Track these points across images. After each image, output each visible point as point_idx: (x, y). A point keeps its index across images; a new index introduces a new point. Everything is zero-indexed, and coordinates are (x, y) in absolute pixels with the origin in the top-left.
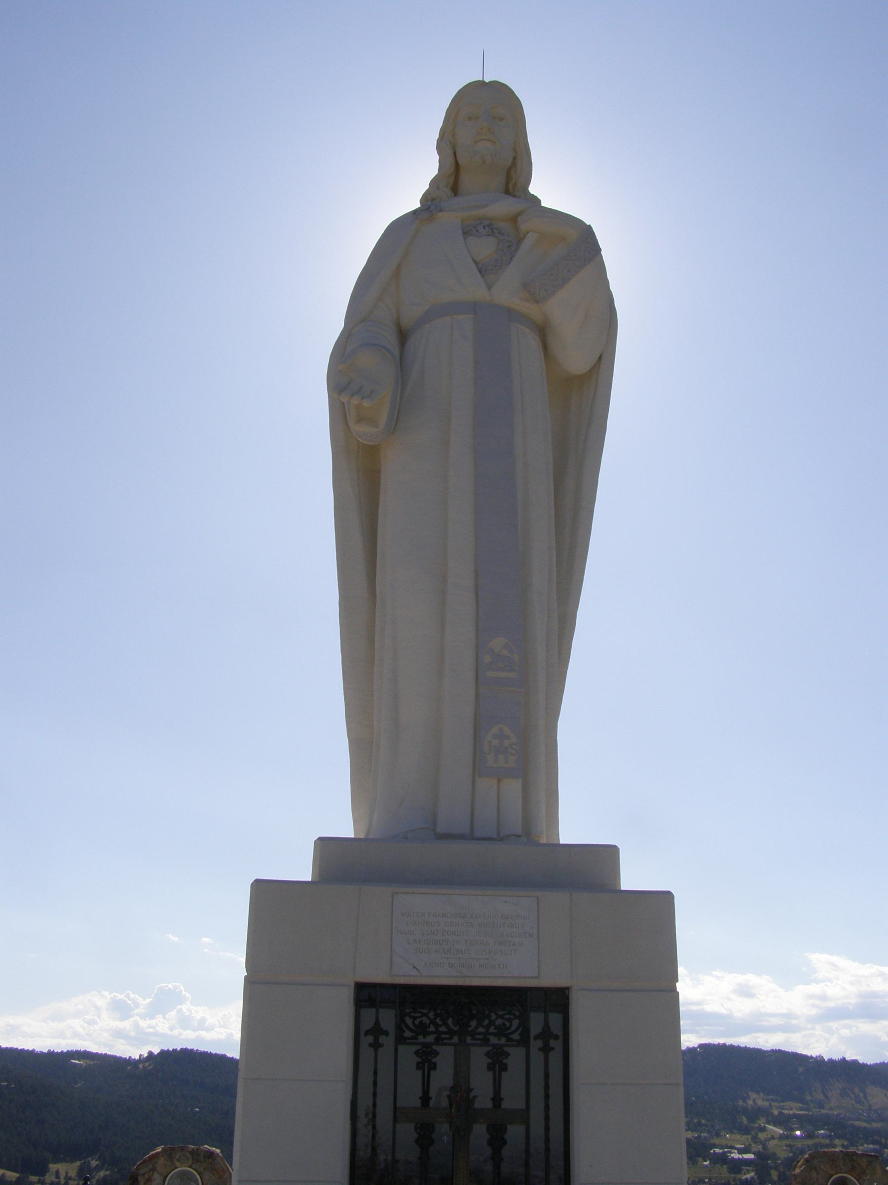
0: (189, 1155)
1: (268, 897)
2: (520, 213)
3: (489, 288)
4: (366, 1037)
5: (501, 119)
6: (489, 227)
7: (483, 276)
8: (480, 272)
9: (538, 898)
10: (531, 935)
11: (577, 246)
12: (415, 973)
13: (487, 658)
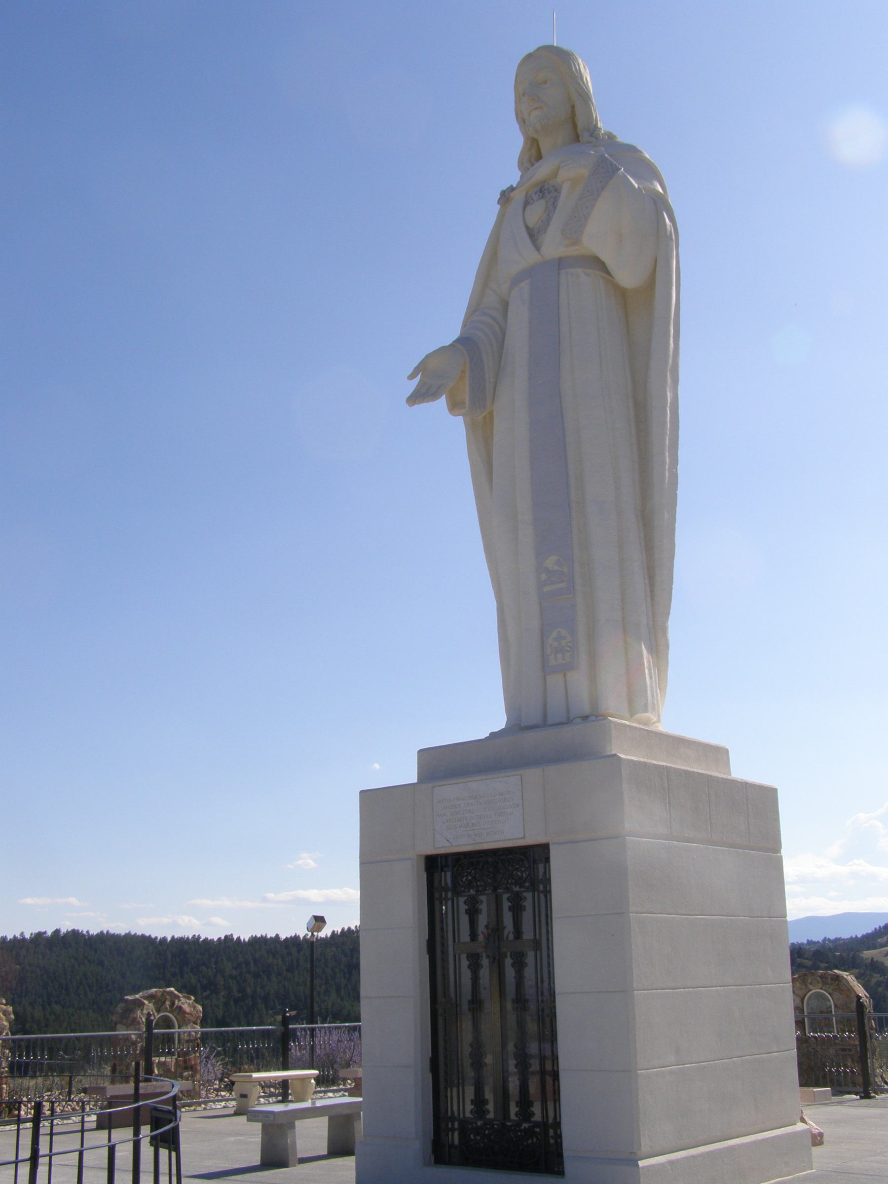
0: (819, 979)
1: (373, 802)
3: (538, 249)
4: (433, 896)
5: (545, 82)
10: (518, 805)
12: (448, 844)
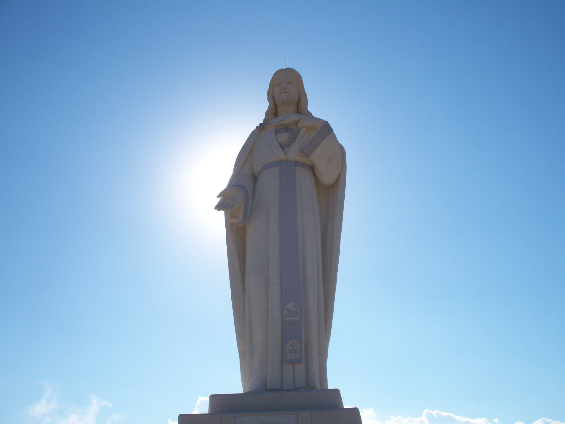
2: (299, 121)
3: (286, 154)
5: (291, 83)
6: (286, 128)
7: (283, 150)
8: (282, 147)
9: (297, 415)
11: (325, 130)
13: (286, 312)
